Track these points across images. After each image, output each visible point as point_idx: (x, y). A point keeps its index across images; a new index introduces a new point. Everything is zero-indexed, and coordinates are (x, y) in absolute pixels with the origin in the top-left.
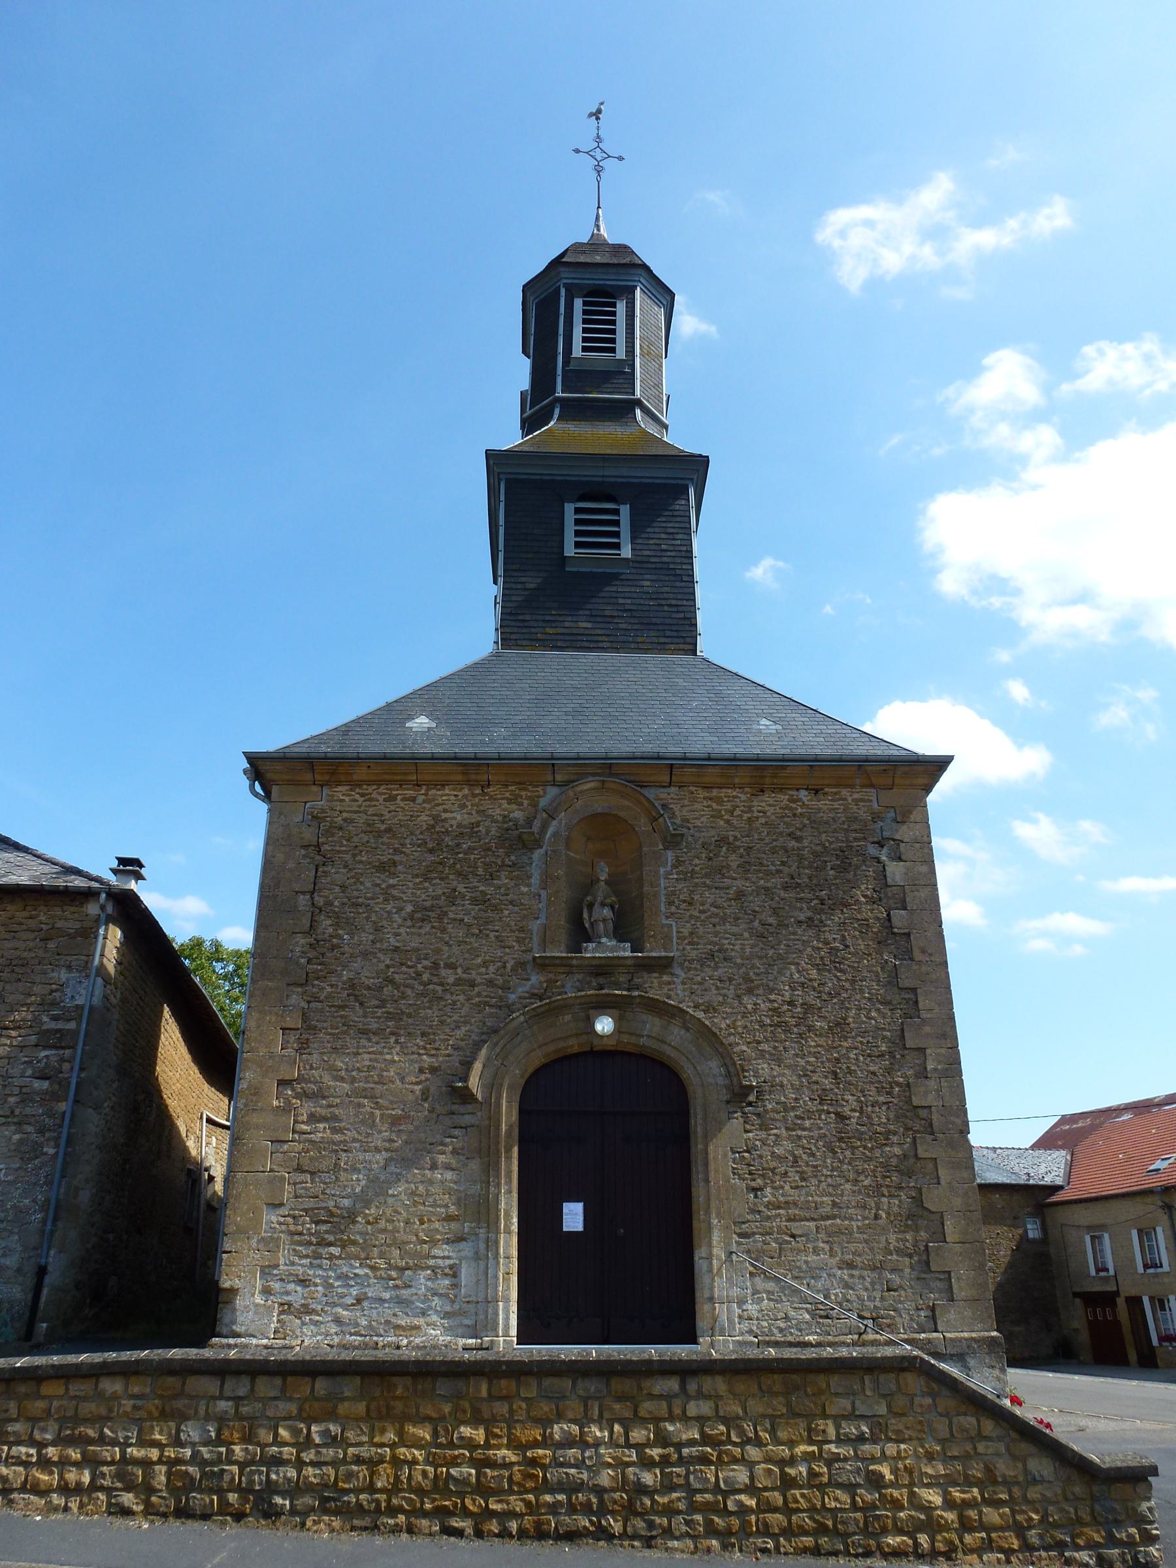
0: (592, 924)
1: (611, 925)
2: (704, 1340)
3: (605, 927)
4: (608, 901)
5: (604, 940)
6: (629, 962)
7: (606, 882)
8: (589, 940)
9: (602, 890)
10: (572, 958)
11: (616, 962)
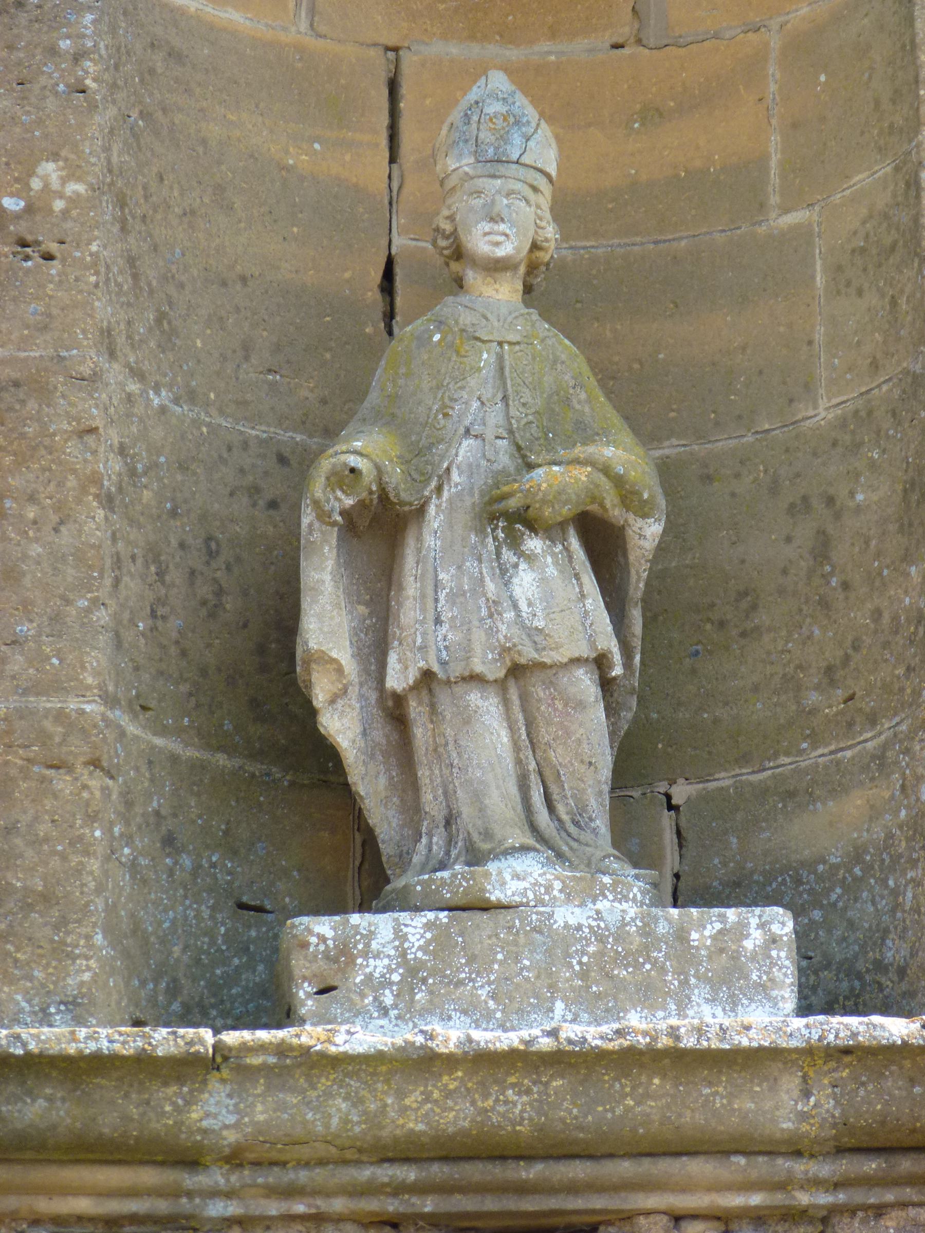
0: (395, 711)
1: (587, 740)
2: (602, 645)
3: (529, 734)
4: (557, 480)
5: (517, 877)
6: (785, 1107)
7: (538, 281)
8: (367, 880)
9: (488, 382)
10: (190, 1068)
11: (648, 1105)
